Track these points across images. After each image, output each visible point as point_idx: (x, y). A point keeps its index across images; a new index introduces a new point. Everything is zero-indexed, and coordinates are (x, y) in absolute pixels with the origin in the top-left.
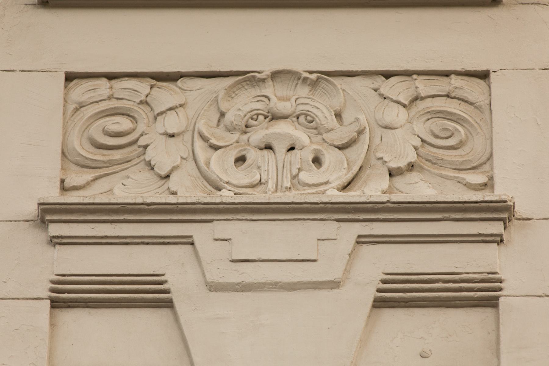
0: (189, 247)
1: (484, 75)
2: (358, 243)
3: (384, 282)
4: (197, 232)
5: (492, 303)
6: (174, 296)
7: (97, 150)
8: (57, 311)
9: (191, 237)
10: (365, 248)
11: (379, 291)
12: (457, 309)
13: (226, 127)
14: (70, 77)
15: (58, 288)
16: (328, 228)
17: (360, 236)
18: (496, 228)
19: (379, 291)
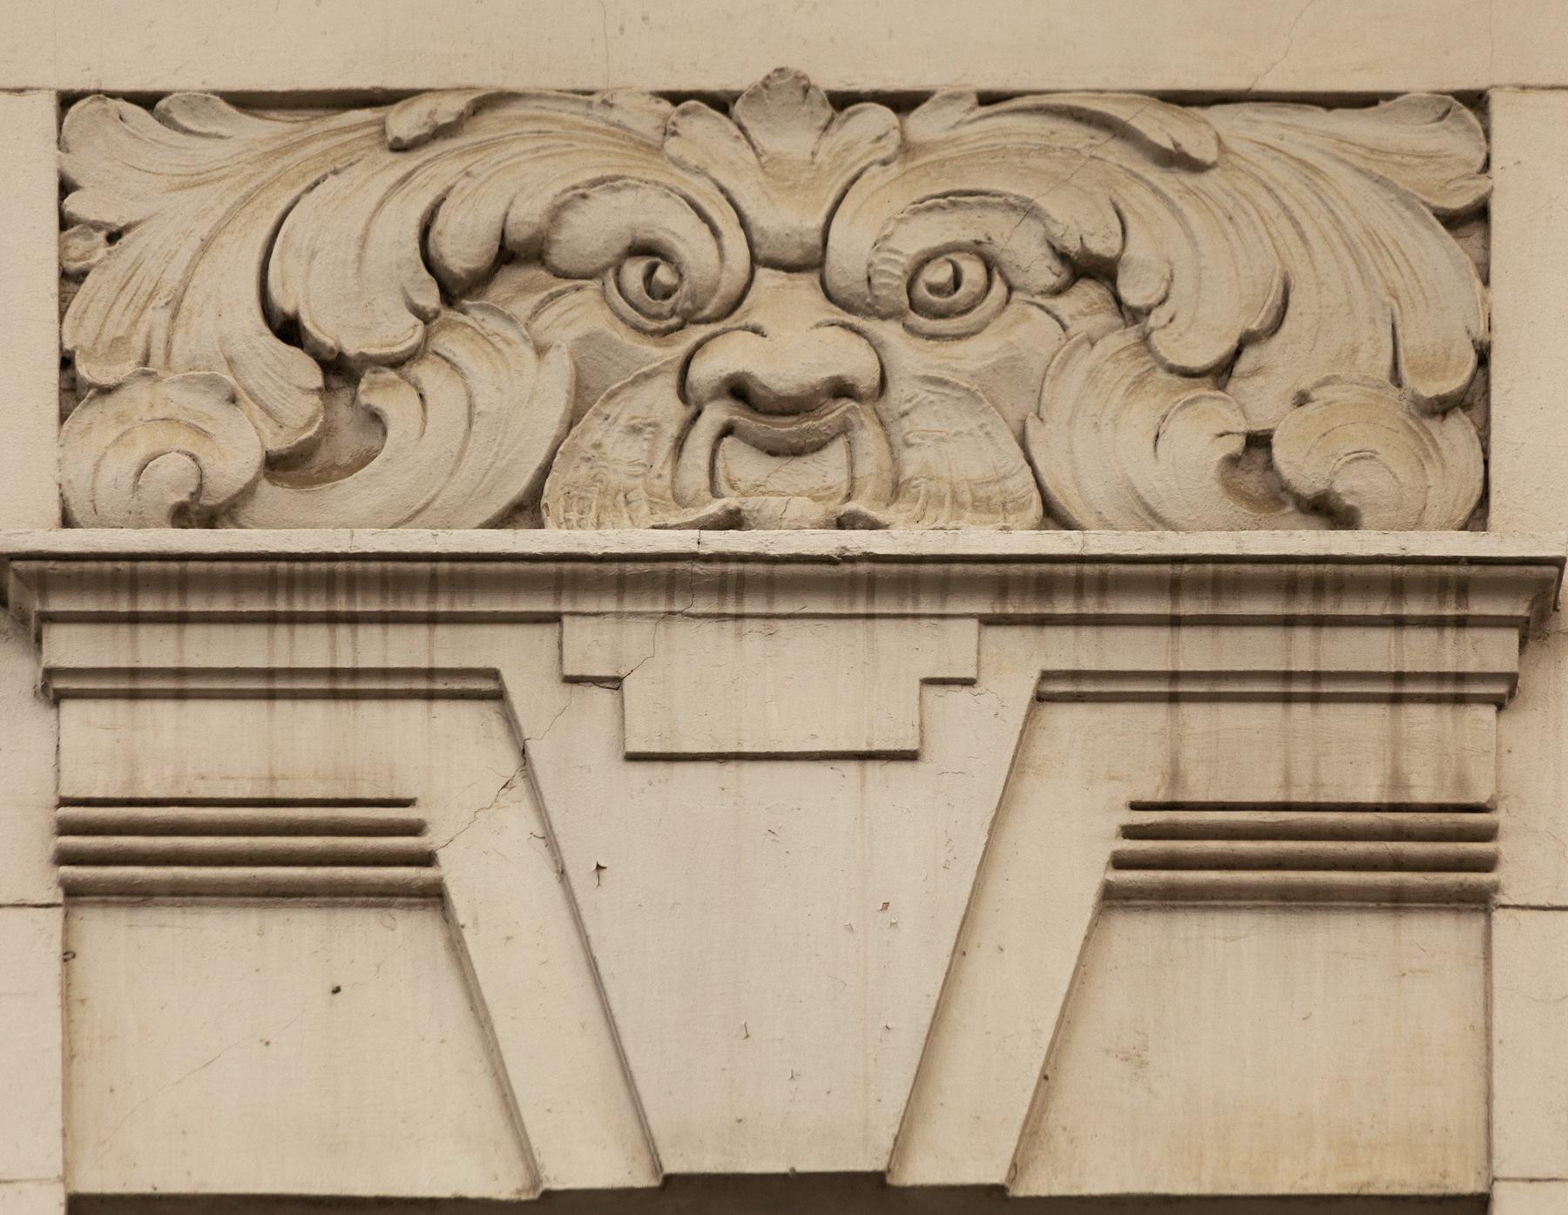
0: (488, 709)
1: (1476, 101)
2: (1041, 698)
3: (1130, 832)
4: (516, 655)
5: (1479, 902)
6: (453, 871)
7: (1278, 336)
8: (103, 929)
9: (494, 674)
10: (1065, 718)
11: (1119, 862)
12: (94, 550)
13: (1053, 247)
14: (67, 100)
15: (133, 878)
16: (953, 642)
17: (1046, 676)
18: (1494, 651)
19: (1119, 862)
